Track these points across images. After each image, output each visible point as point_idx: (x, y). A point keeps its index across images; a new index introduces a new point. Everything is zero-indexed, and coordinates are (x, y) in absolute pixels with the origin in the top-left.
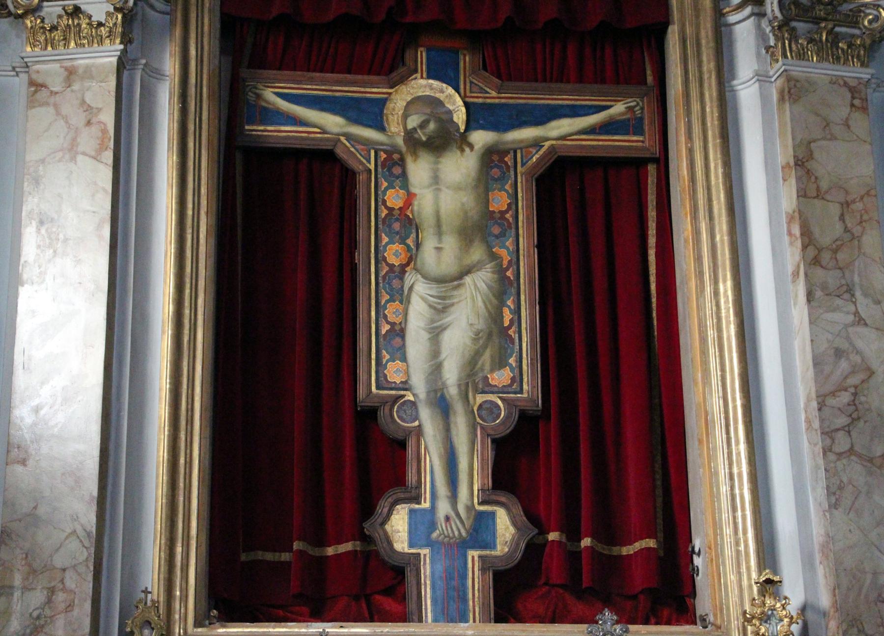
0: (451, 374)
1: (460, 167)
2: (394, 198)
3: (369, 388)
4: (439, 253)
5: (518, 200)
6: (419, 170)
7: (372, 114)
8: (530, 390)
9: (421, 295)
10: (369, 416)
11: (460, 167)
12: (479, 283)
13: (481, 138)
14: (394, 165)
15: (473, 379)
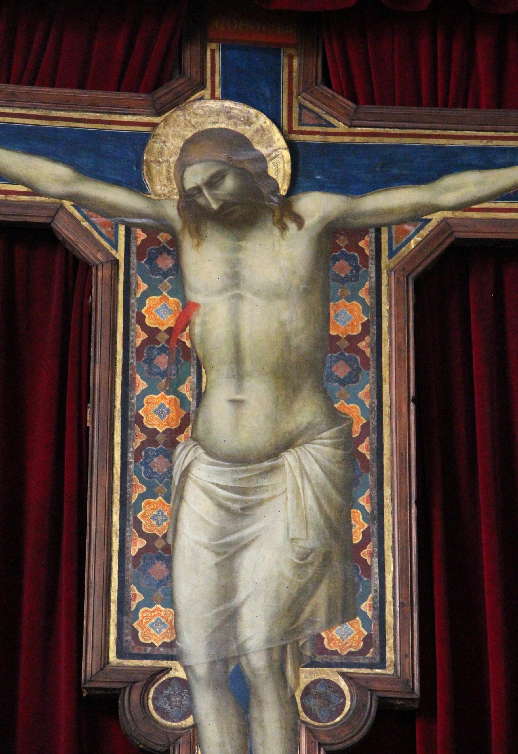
0: (255, 630)
1: (278, 257)
2: (159, 311)
3: (105, 654)
4: (237, 410)
5: (380, 316)
6: (204, 262)
7: (120, 160)
8: (398, 660)
9: (203, 482)
10: (102, 707)
11: (278, 257)
12: (311, 464)
13: (317, 206)
14: (159, 251)
15: (294, 642)
